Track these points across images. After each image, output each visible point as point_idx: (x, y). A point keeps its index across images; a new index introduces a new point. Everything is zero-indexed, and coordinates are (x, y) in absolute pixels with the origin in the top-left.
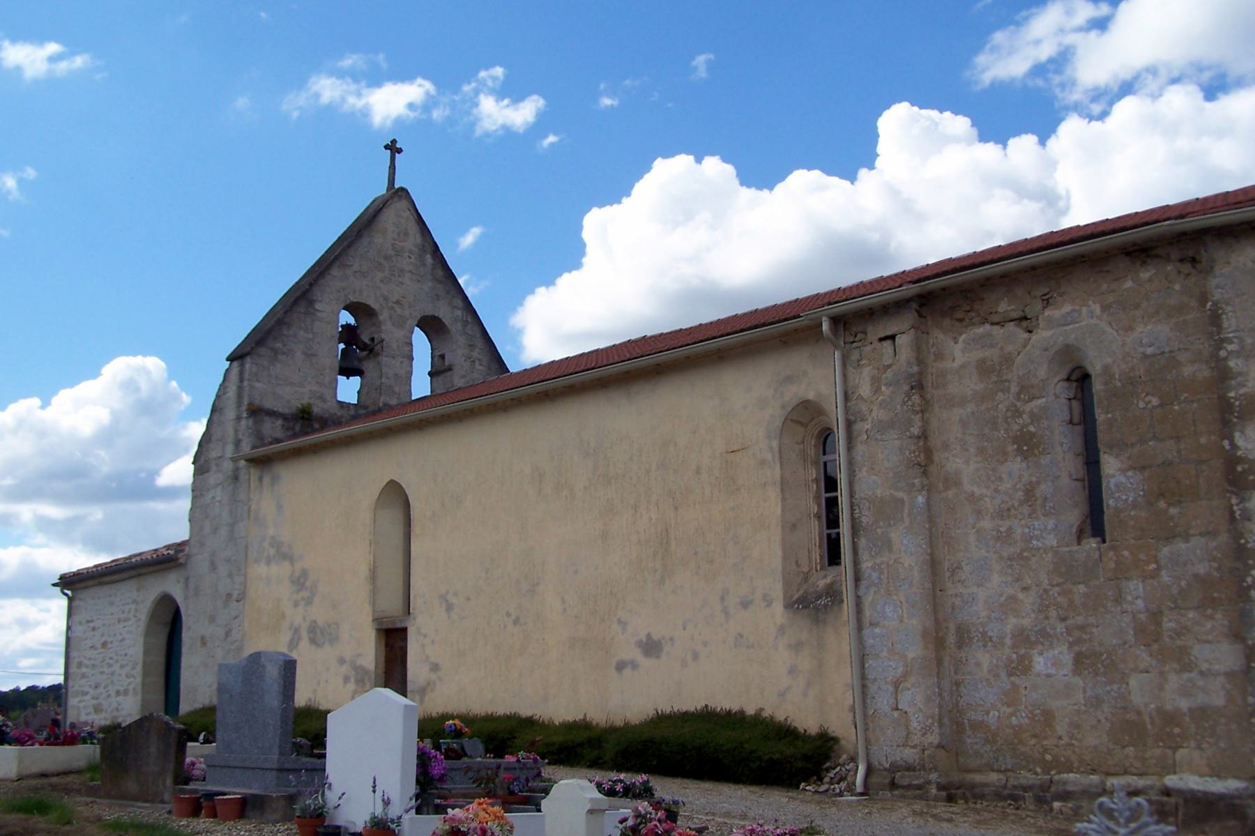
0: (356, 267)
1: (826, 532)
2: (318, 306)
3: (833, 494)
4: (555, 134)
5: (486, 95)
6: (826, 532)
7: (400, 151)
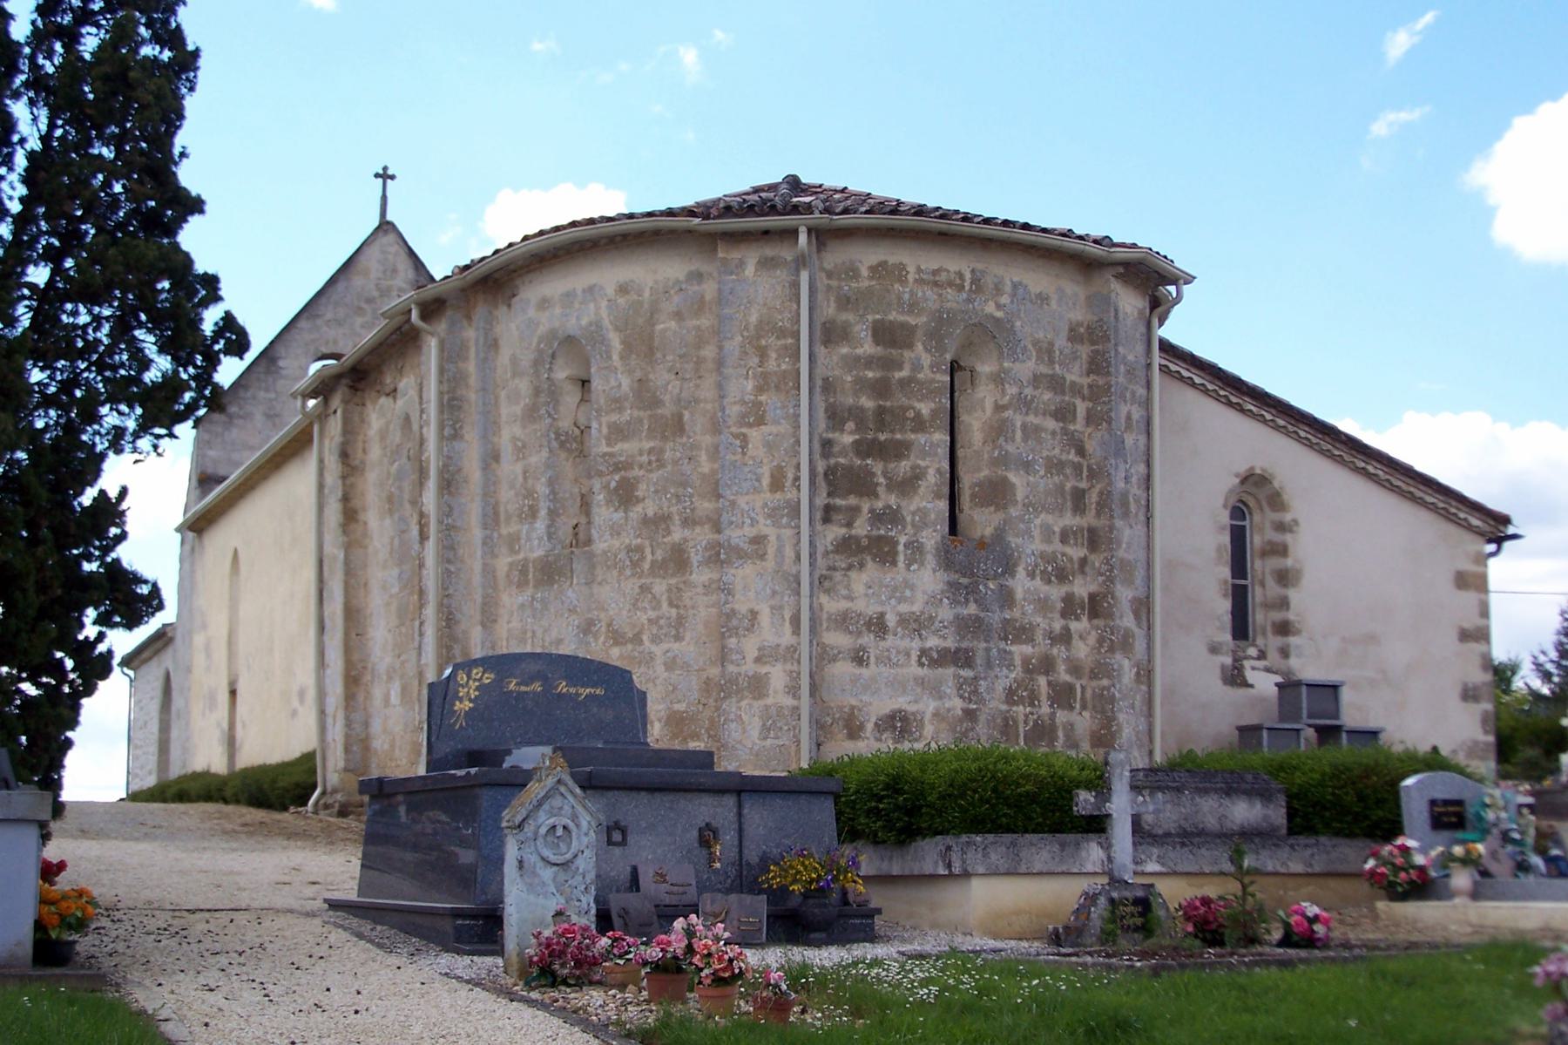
0: (329, 316)
1: (1247, 523)
2: (281, 363)
3: (1243, 582)
4: (22, 373)
5: (36, 265)
6: (1247, 523)
7: (392, 177)
